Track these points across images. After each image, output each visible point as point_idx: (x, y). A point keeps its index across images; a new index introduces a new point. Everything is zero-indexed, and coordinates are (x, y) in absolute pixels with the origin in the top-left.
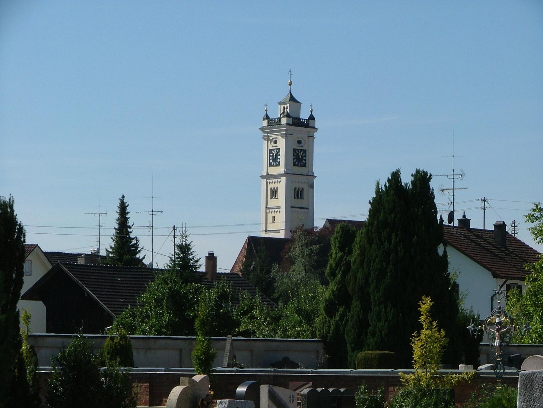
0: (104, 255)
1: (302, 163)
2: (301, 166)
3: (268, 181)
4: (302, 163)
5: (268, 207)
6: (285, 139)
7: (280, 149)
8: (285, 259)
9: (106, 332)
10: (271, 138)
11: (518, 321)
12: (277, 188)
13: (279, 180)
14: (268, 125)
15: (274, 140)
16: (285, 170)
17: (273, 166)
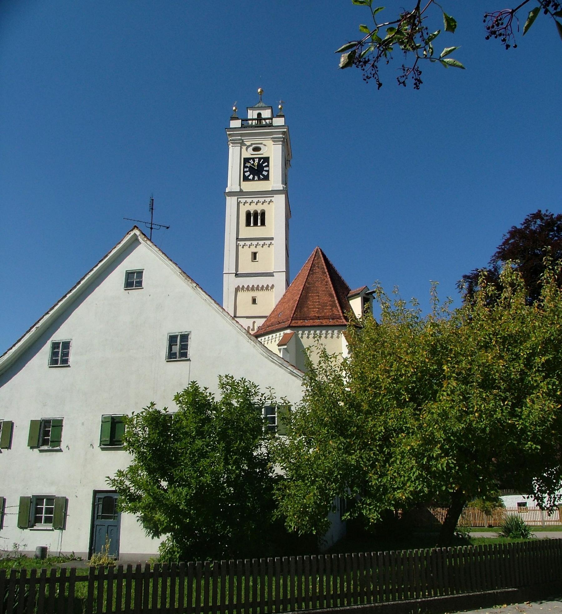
1: (261, 176)
2: (259, 179)
3: (243, 200)
4: (261, 176)
10: (248, 143)
13: (268, 200)
15: (254, 146)
17: (250, 180)
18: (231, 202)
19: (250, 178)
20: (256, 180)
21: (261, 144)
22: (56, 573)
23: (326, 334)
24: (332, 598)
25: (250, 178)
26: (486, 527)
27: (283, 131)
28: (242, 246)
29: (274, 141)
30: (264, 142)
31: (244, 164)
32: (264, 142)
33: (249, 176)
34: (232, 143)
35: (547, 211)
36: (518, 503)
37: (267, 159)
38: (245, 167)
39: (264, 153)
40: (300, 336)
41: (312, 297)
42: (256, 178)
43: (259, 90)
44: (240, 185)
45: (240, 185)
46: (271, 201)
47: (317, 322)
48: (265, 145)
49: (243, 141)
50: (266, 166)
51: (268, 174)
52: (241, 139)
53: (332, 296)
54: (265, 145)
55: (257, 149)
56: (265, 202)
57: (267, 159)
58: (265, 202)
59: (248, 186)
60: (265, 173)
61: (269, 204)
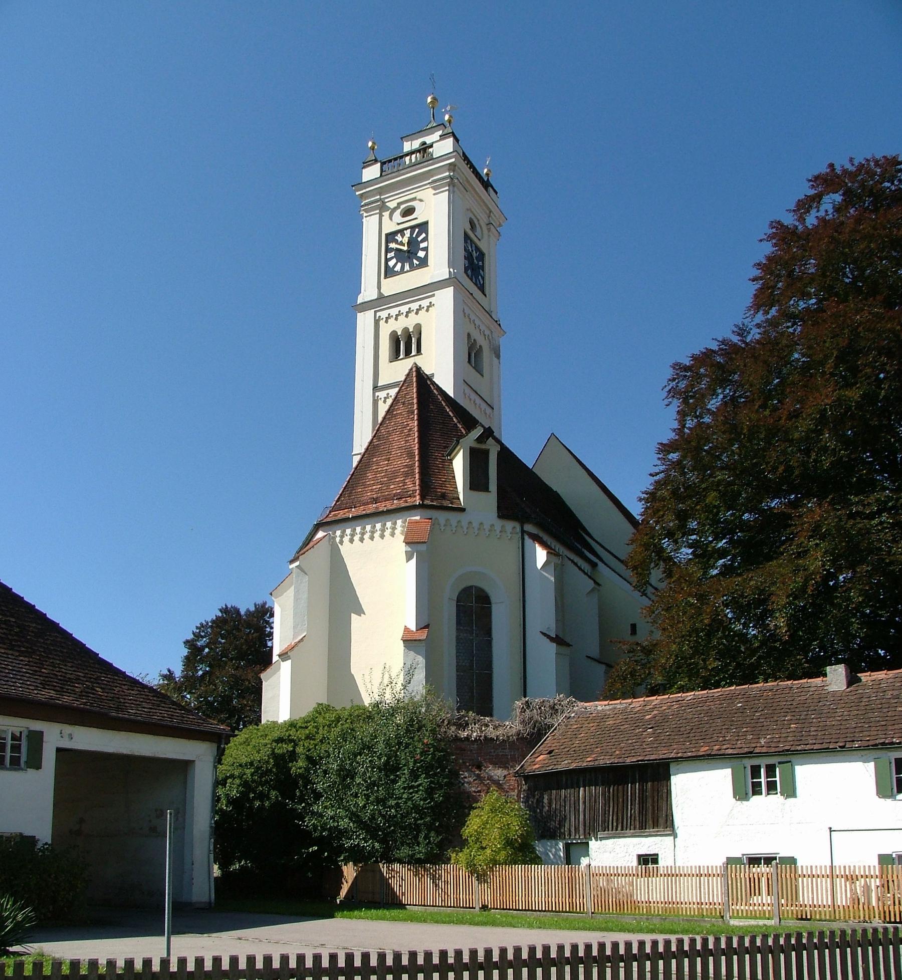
0: (132, 669)
2: (413, 268)
3: (383, 314)
5: (379, 385)
6: (449, 190)
7: (426, 223)
8: (785, 510)
9: (413, 474)
10: (392, 205)
11: (774, 503)
12: (418, 328)
13: (425, 303)
14: (381, 174)
15: (402, 207)
16: (451, 270)
17: (397, 274)
18: (365, 320)
19: (396, 269)
20: (407, 271)
21: (414, 199)
22: (389, 885)
23: (383, 530)
24: (771, 952)
25: (396, 269)
26: (477, 909)
27: (450, 164)
28: (383, 399)
29: (434, 188)
30: (419, 195)
31: (387, 242)
32: (419, 195)
33: (395, 266)
34: (366, 212)
35: (851, 160)
36: (639, 856)
37: (423, 227)
38: (388, 250)
39: (420, 216)
40: (338, 539)
41: (377, 463)
42: (407, 267)
43: (429, 100)
44: (379, 287)
45: (379, 287)
46: (431, 305)
47: (372, 508)
48: (421, 200)
49: (384, 203)
50: (424, 240)
51: (427, 255)
52: (380, 199)
53: (411, 455)
54: (421, 200)
55: (409, 212)
56: (420, 308)
57: (423, 227)
58: (420, 308)
59: (392, 286)
60: (421, 254)
61: (427, 310)
